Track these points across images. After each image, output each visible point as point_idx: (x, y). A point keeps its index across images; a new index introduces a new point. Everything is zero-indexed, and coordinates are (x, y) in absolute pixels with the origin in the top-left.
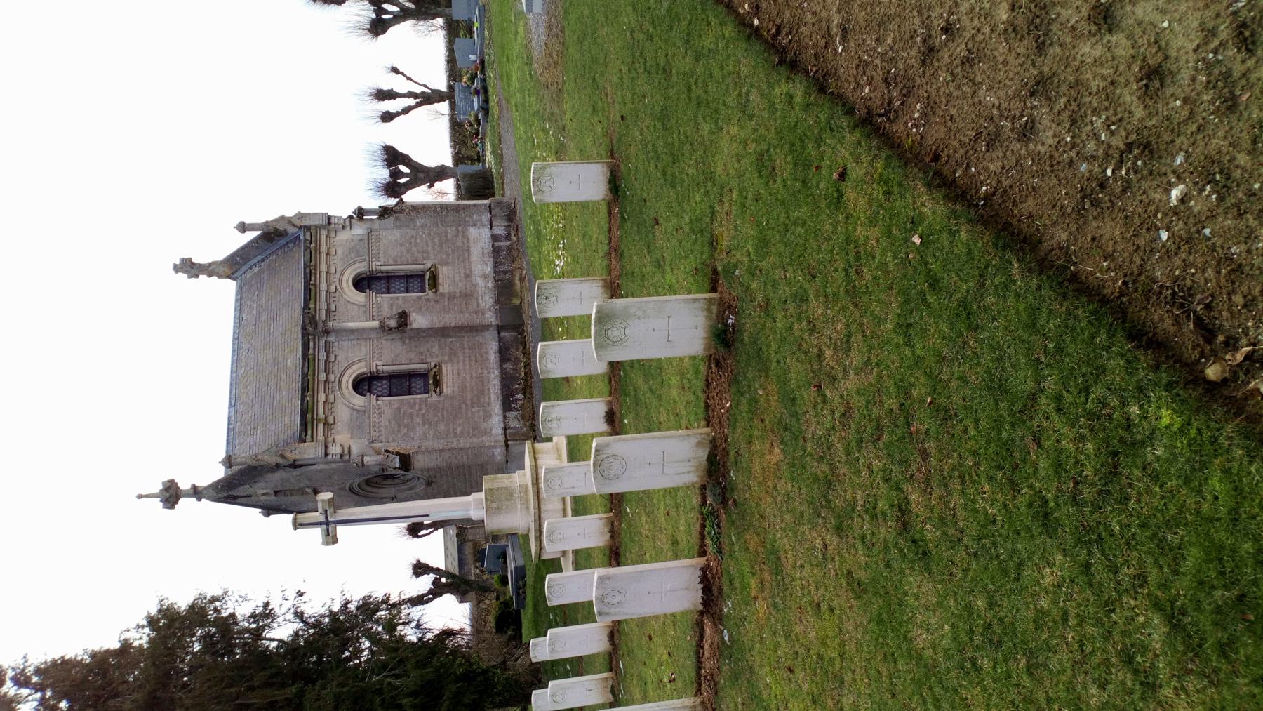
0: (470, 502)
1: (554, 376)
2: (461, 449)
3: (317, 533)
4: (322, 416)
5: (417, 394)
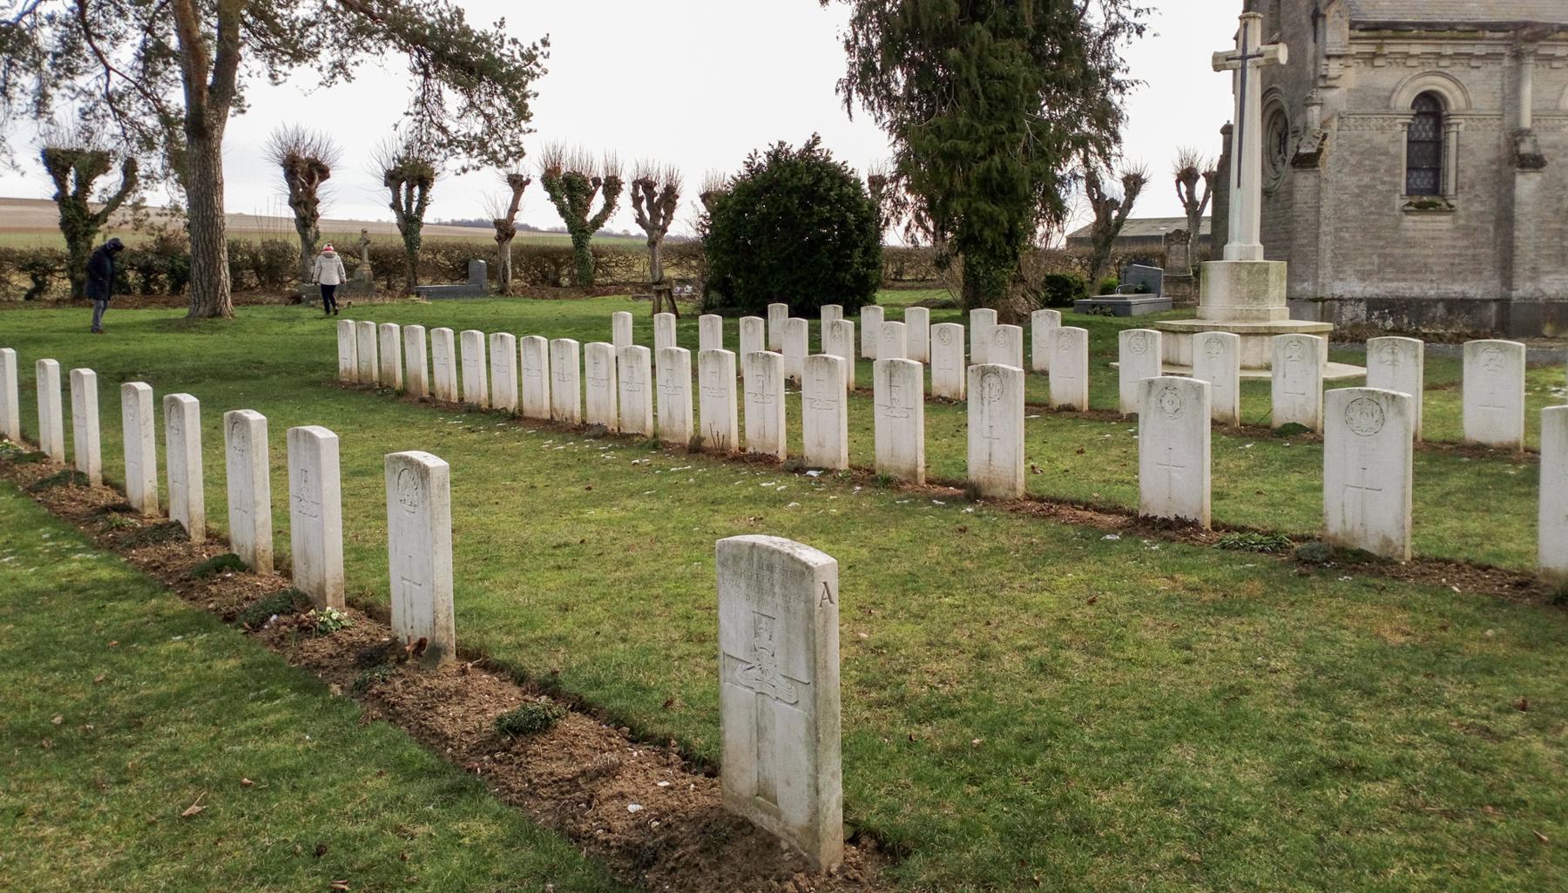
0: (1250, 242)
1: (1466, 360)
2: (1317, 237)
3: (1230, 46)
4: (1386, 50)
5: (1408, 179)
